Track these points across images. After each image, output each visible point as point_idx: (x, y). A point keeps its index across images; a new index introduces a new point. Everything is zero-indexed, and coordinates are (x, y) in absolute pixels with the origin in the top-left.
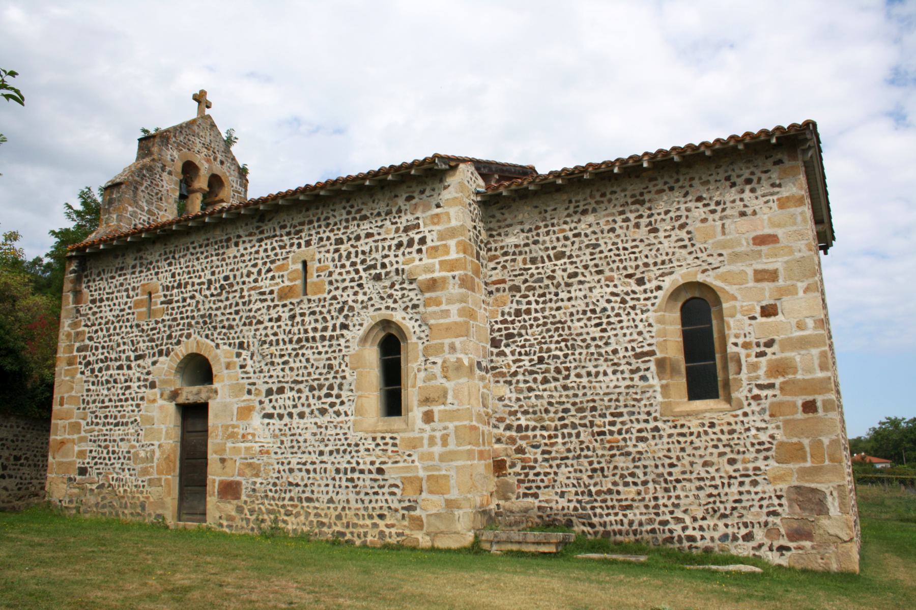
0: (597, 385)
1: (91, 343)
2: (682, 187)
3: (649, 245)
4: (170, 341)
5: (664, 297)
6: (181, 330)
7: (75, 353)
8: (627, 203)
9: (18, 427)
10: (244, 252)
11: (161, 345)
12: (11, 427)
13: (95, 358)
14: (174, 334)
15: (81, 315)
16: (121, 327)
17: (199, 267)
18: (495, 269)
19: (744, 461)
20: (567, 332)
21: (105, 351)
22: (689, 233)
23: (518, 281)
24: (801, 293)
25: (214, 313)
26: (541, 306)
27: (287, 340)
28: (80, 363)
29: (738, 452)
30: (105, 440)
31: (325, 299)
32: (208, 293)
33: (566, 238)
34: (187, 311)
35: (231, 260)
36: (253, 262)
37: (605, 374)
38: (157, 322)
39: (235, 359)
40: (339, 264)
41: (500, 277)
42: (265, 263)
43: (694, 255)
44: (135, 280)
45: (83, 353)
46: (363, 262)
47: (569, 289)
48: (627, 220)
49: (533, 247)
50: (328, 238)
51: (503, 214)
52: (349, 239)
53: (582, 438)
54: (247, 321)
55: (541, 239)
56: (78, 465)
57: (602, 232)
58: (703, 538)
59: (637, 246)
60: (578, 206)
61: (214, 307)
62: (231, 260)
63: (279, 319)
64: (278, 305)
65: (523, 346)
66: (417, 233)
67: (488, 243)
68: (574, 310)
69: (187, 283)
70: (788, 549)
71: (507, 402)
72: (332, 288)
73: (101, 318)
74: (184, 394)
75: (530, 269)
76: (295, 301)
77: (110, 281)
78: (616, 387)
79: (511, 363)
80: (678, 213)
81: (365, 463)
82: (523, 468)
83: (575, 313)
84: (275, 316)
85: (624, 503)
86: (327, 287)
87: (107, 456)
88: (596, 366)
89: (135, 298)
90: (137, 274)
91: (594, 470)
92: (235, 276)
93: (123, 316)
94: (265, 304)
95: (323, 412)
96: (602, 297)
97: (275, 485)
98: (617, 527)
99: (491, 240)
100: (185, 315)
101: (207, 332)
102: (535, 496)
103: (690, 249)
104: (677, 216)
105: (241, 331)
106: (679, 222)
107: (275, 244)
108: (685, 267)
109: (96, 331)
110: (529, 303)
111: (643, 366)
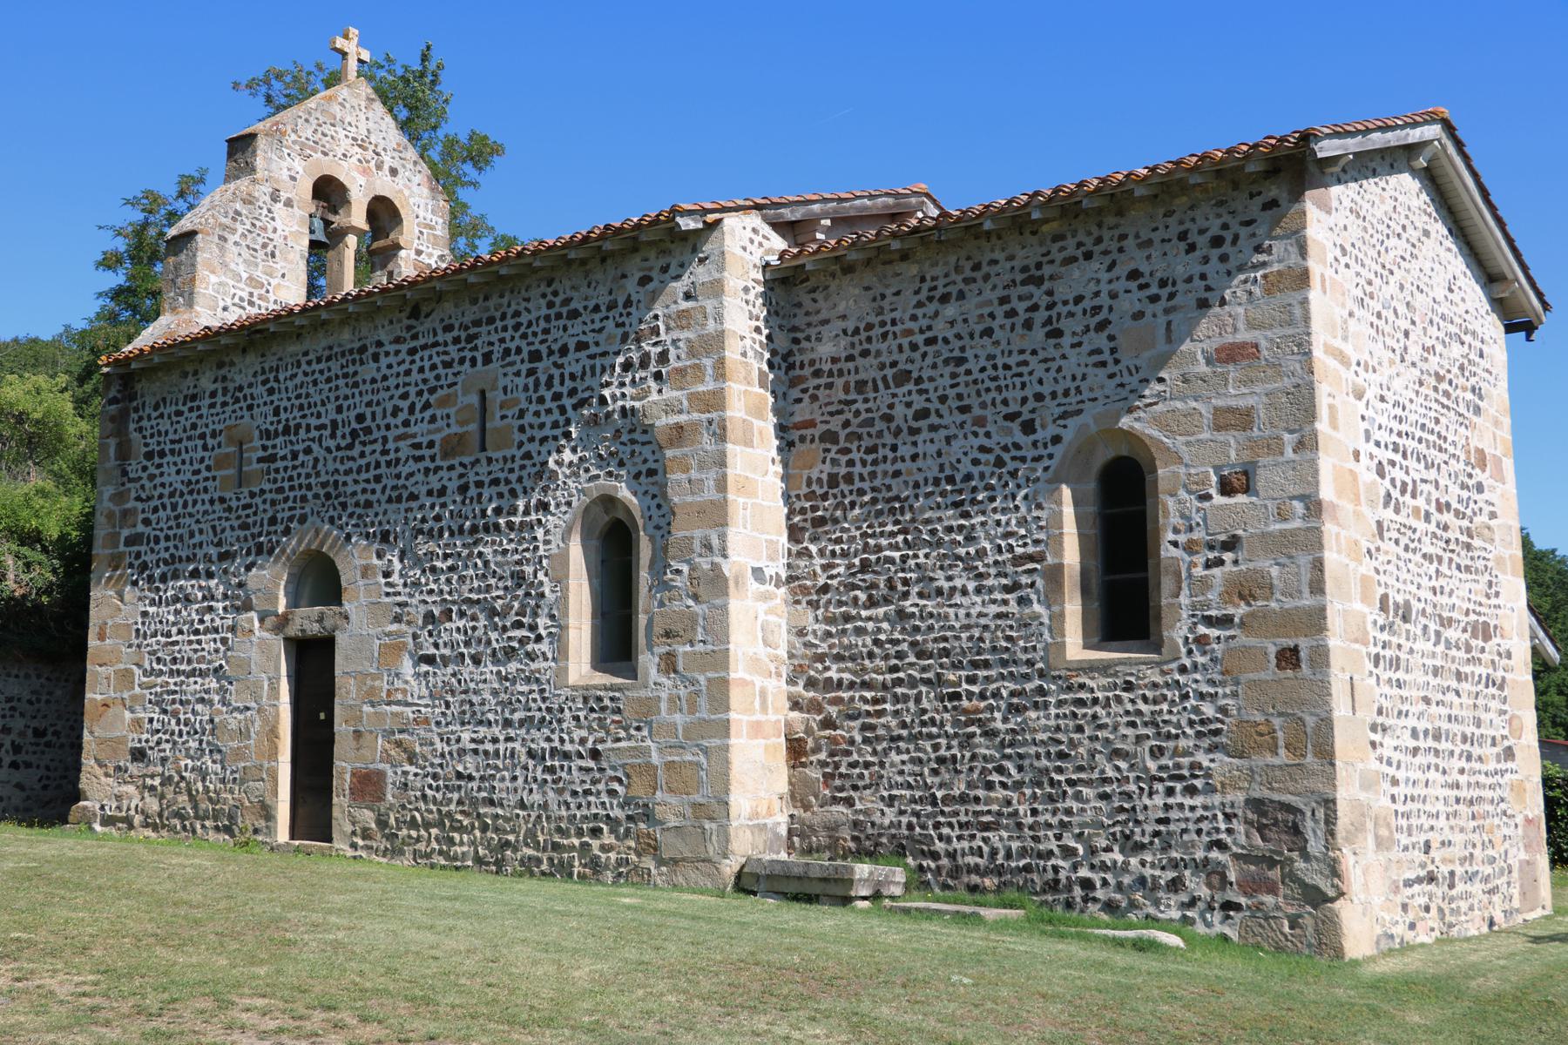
0: (951, 611)
1: (148, 530)
2: (1106, 253)
3: (1045, 360)
4: (272, 529)
5: (1064, 456)
6: (291, 509)
7: (122, 548)
8: (1014, 281)
9: (39, 676)
10: (388, 372)
11: (260, 535)
12: (27, 676)
13: (154, 557)
14: (279, 516)
15: (130, 480)
16: (195, 502)
17: (317, 398)
18: (799, 401)
19: (1176, 753)
20: (908, 517)
21: (171, 544)
22: (1111, 338)
23: (835, 424)
24: (1289, 453)
25: (341, 479)
26: (869, 468)
27: (455, 528)
28: (131, 566)
29: (1169, 736)
30: (174, 702)
31: (513, 457)
32: (332, 444)
33: (914, 347)
34: (299, 475)
35: (368, 386)
36: (401, 390)
37: (964, 592)
38: (252, 495)
39: (375, 561)
40: (534, 397)
41: (808, 417)
42: (420, 393)
43: (1118, 380)
44: (216, 419)
45: (135, 548)
46: (572, 393)
47: (913, 439)
48: (1012, 313)
49: (860, 361)
50: (519, 350)
51: (815, 301)
52: (551, 353)
53: (925, 704)
54: (394, 494)
55: (873, 347)
56: (130, 745)
57: (972, 336)
58: (1105, 883)
59: (1025, 363)
60: (935, 288)
61: (342, 468)
62: (368, 386)
63: (442, 492)
64: (441, 468)
65: (838, 541)
66: (655, 344)
67: (790, 353)
68: (920, 478)
69: (298, 426)
70: (1237, 907)
71: (810, 638)
72: (524, 438)
73: (163, 485)
74: (298, 621)
75: (855, 401)
76: (467, 460)
77: (175, 419)
78: (980, 615)
79: (819, 570)
80: (1097, 302)
81: (572, 741)
82: (832, 754)
83: (922, 483)
84: (437, 486)
85: (985, 819)
86: (517, 436)
87: (177, 729)
88: (950, 578)
89: (217, 451)
90: (218, 409)
91: (941, 761)
92: (373, 414)
93: (197, 482)
94: (421, 465)
95: (510, 653)
96: (965, 454)
97: (435, 777)
98: (972, 860)
99: (795, 348)
100: (296, 483)
101: (331, 513)
102: (849, 802)
103: (1111, 368)
104: (1093, 308)
105: (385, 513)
106: (1098, 318)
107: (436, 360)
108: (1101, 401)
109: (156, 510)
110: (851, 463)
111: (1025, 580)
